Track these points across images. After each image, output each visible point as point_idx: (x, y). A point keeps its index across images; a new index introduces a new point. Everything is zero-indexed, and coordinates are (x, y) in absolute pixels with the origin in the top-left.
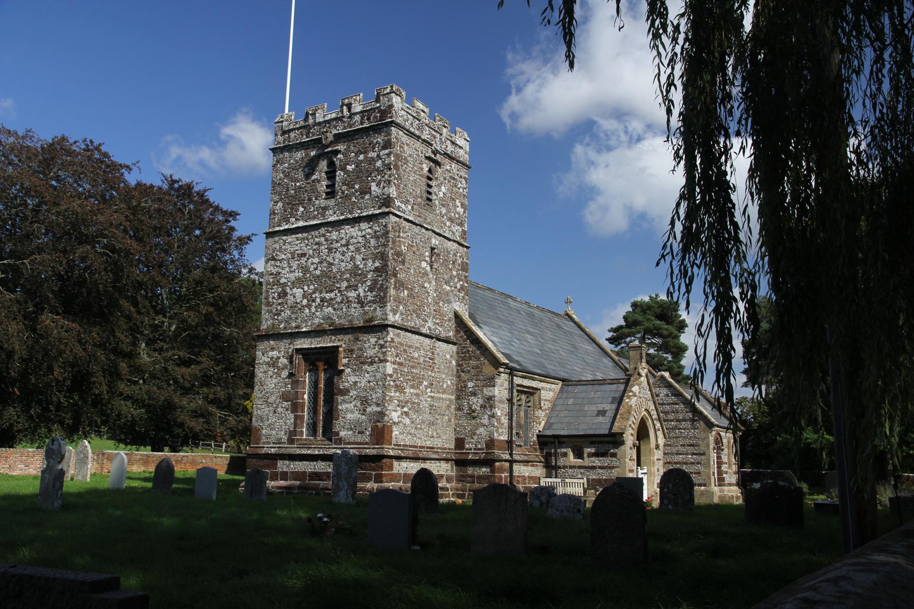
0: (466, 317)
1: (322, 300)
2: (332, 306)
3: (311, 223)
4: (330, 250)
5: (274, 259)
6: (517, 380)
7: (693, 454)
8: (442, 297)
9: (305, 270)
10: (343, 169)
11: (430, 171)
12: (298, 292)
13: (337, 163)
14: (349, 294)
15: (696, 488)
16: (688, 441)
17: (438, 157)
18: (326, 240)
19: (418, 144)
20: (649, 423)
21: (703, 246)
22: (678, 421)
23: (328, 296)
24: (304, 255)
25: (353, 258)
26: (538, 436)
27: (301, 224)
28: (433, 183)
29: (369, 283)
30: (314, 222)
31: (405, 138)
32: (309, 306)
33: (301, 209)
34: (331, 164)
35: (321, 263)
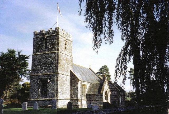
0: (72, 71)
1: (45, 68)
2: (47, 70)
3: (41, 53)
4: (46, 59)
5: (34, 60)
6: (82, 83)
7: (116, 97)
8: (68, 67)
9: (41, 62)
10: (49, 43)
11: (65, 43)
12: (39, 67)
13: (47, 42)
14: (51, 67)
15: (83, 108)
16: (115, 95)
17: (67, 40)
18: (46, 57)
19: (63, 38)
20: (107, 91)
21: (93, 17)
22: (113, 90)
23: (46, 68)
24: (41, 59)
25: (51, 60)
26: (86, 94)
27: (40, 53)
28: (66, 45)
29: (54, 65)
30: (43, 53)
31: (61, 37)
32: (42, 70)
33: (40, 50)
34: (46, 42)
35: (44, 61)
